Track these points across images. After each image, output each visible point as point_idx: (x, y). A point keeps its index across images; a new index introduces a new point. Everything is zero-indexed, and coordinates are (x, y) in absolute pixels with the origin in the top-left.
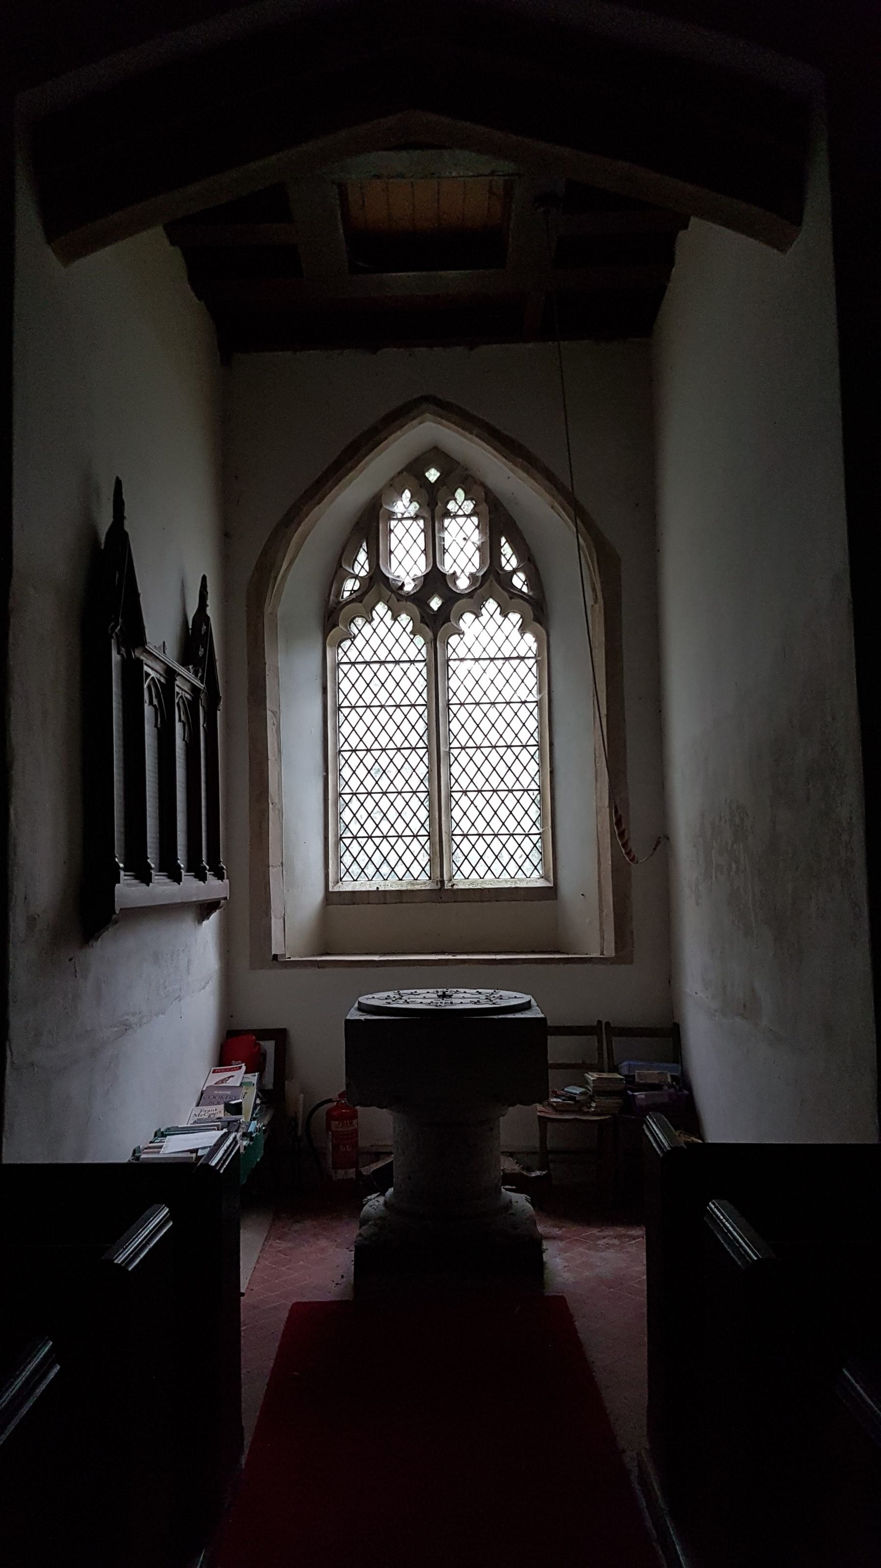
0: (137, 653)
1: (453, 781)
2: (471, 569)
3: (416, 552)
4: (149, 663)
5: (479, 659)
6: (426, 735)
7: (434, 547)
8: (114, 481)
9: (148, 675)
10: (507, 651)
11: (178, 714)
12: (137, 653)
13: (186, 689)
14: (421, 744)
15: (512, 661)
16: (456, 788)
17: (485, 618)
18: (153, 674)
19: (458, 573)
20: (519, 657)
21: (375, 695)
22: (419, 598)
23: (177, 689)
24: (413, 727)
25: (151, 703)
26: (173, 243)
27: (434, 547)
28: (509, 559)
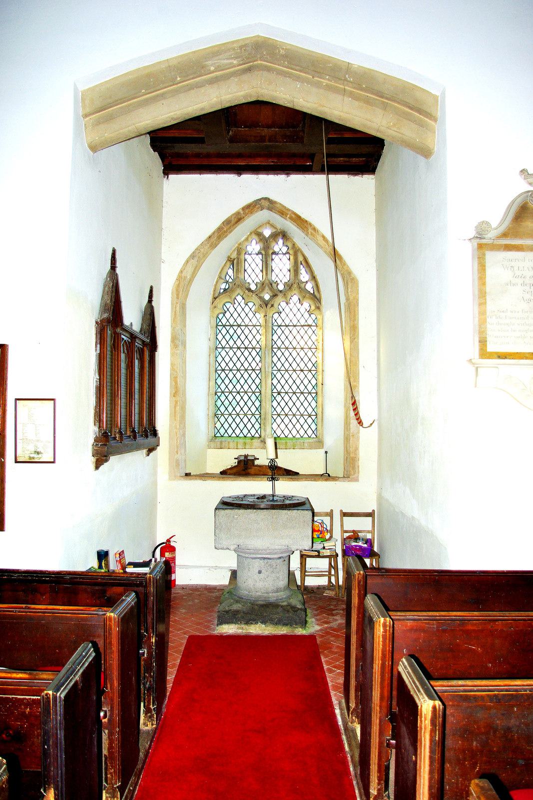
0: (118, 330)
1: (274, 343)
2: (286, 280)
3: (258, 271)
4: (124, 334)
5: (288, 326)
6: (260, 385)
7: (266, 266)
8: (104, 467)
9: (123, 339)
10: (303, 322)
11: (136, 355)
12: (118, 330)
13: (140, 343)
14: (257, 390)
15: (304, 327)
16: (275, 346)
17: (291, 305)
18: (125, 338)
19: (279, 282)
20: (309, 325)
21: (234, 431)
22: (258, 293)
23: (136, 344)
24: (253, 426)
25: (124, 352)
26: (155, 151)
27: (266, 266)
28: (304, 276)
